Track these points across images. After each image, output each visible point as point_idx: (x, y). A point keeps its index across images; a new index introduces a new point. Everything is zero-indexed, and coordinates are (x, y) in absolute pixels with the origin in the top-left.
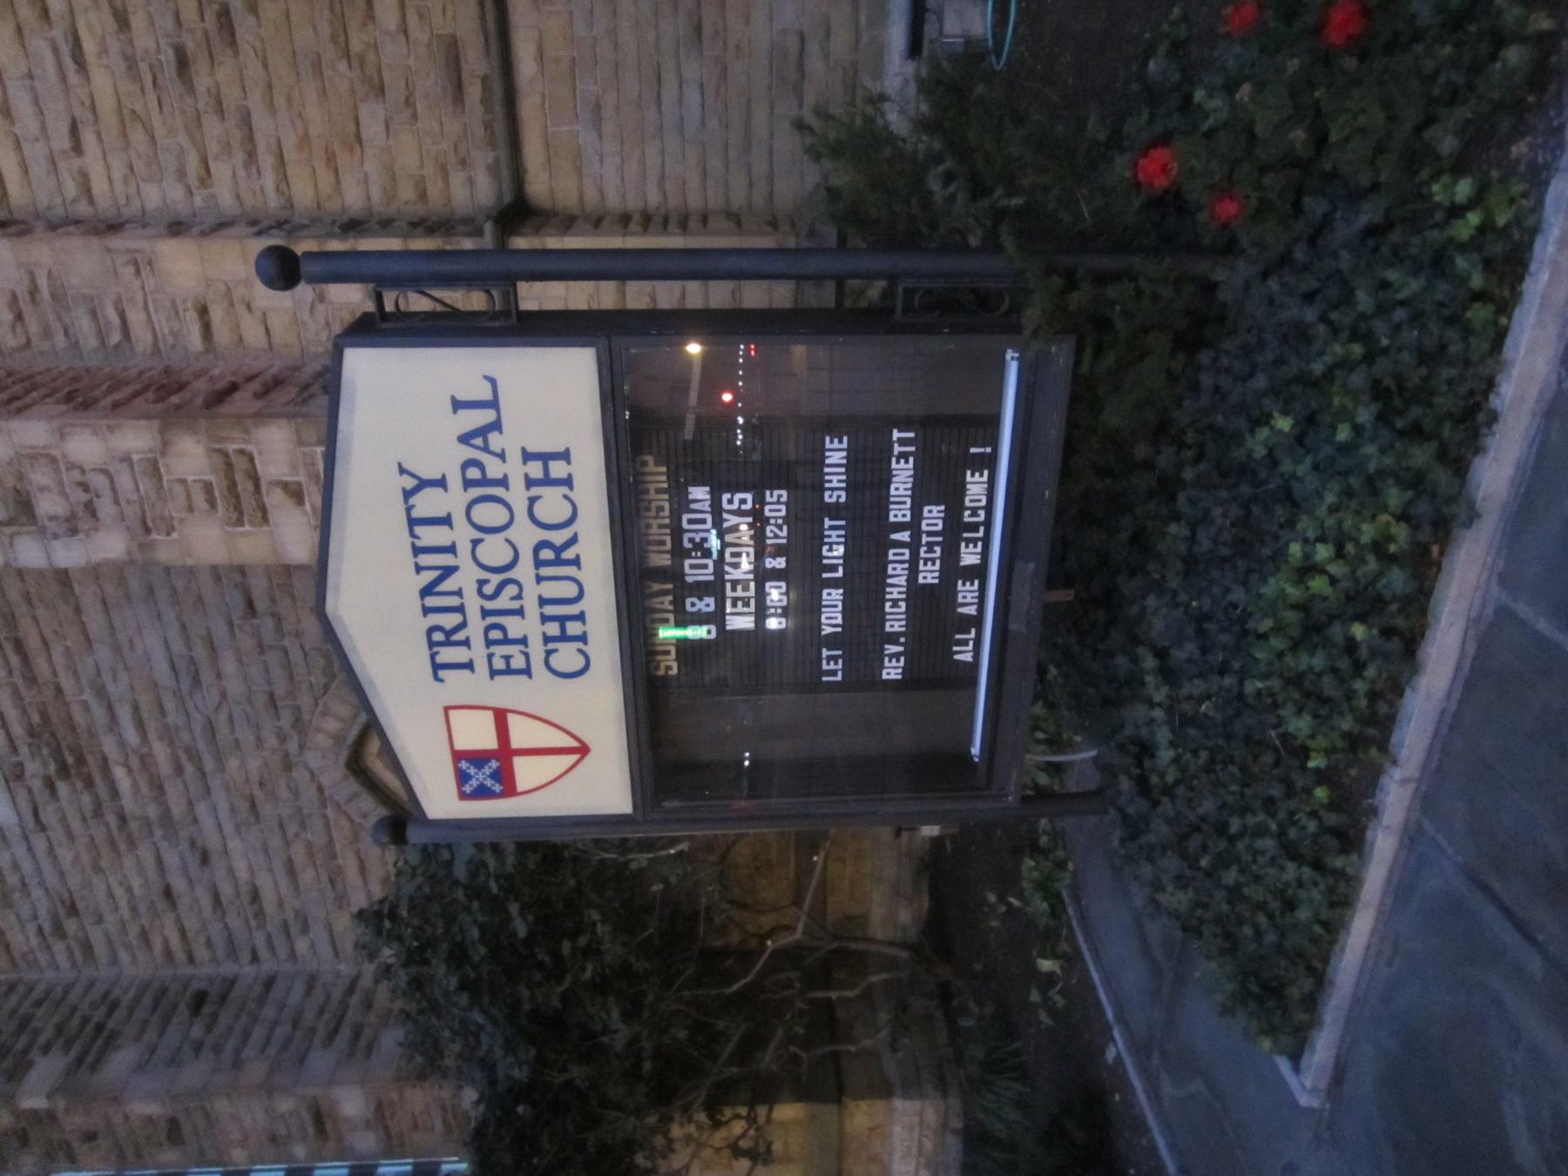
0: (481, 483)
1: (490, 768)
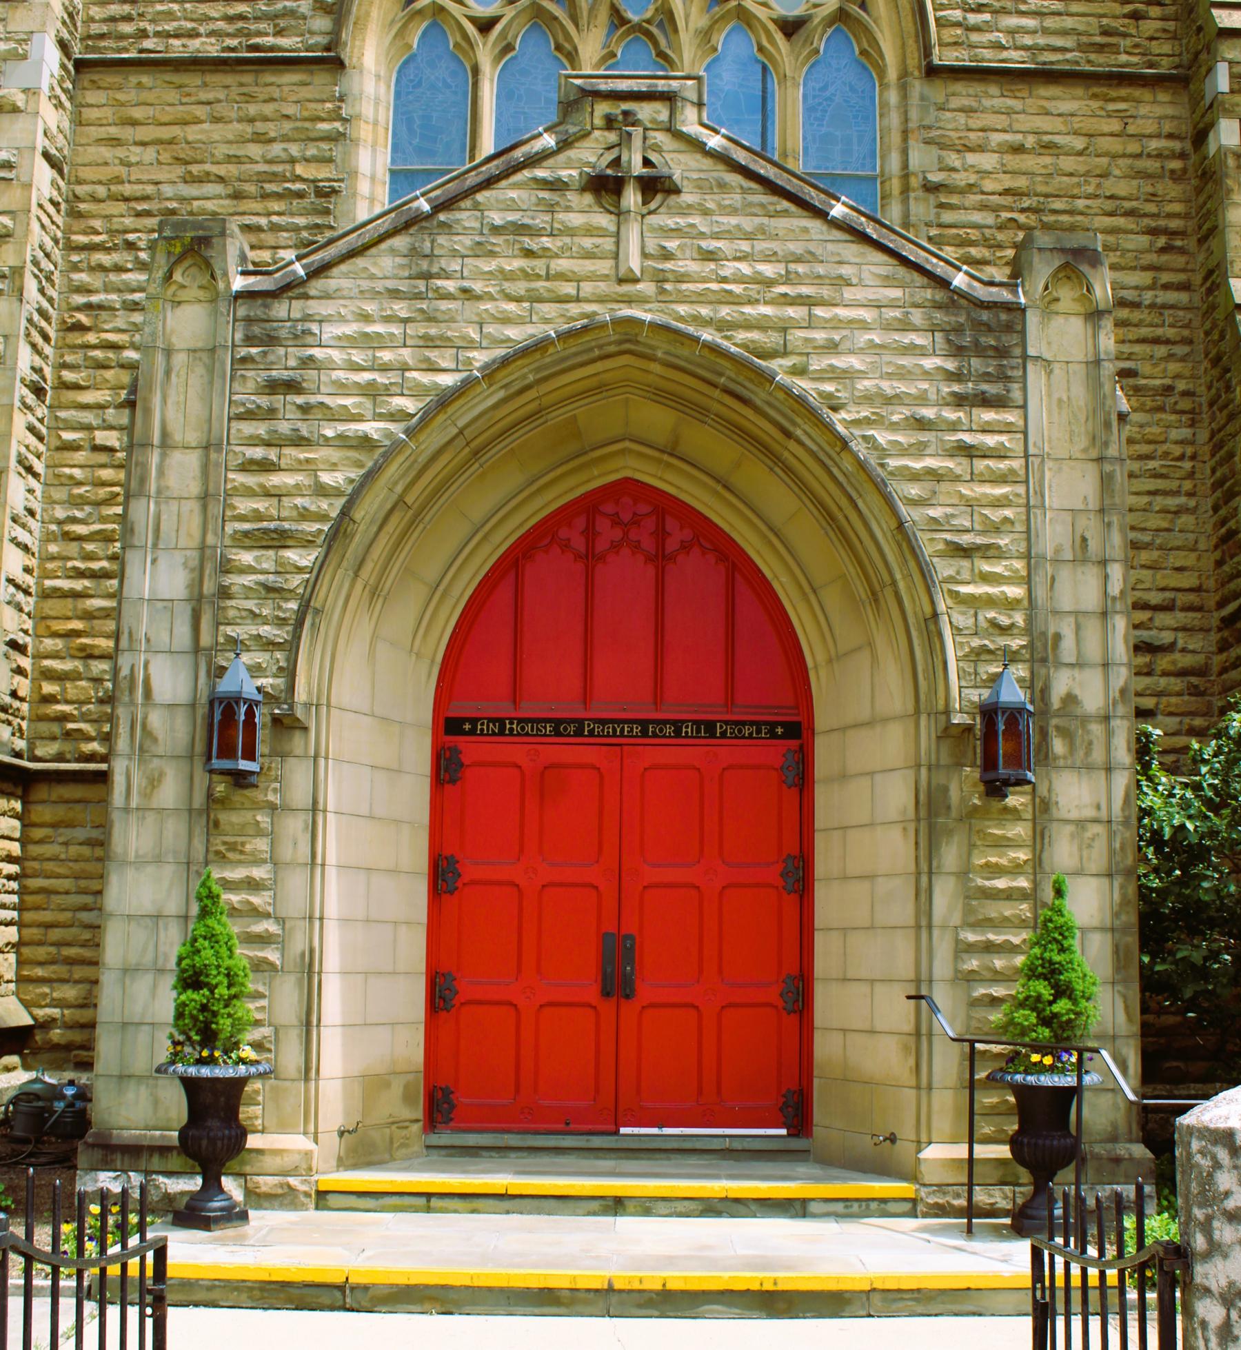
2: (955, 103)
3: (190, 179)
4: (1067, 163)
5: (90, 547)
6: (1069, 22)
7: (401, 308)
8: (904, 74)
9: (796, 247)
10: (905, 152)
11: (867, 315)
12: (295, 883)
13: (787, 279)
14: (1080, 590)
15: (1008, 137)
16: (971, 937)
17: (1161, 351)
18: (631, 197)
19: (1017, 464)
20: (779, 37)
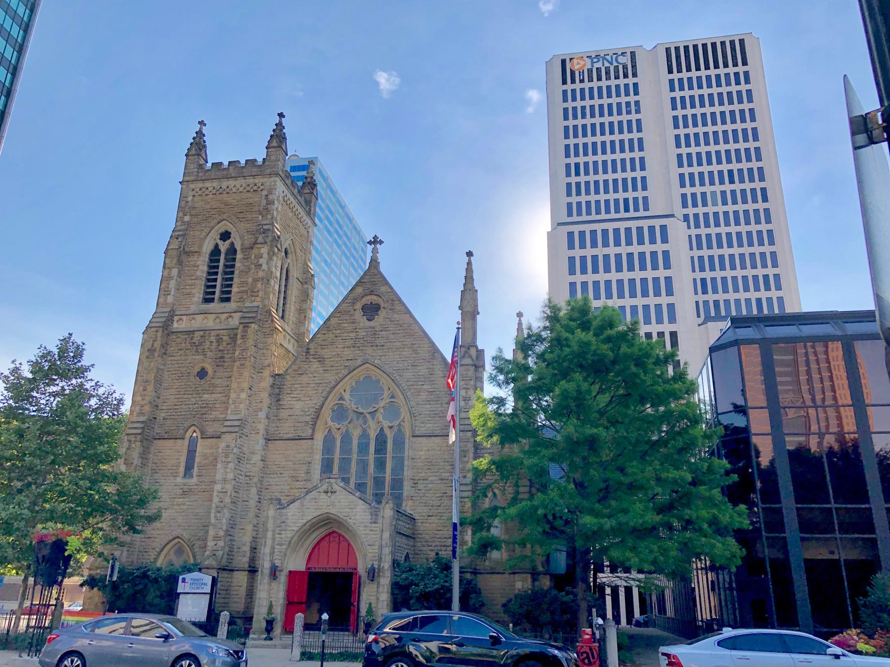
1: (184, 580)
3: (287, 461)
14: (387, 551)
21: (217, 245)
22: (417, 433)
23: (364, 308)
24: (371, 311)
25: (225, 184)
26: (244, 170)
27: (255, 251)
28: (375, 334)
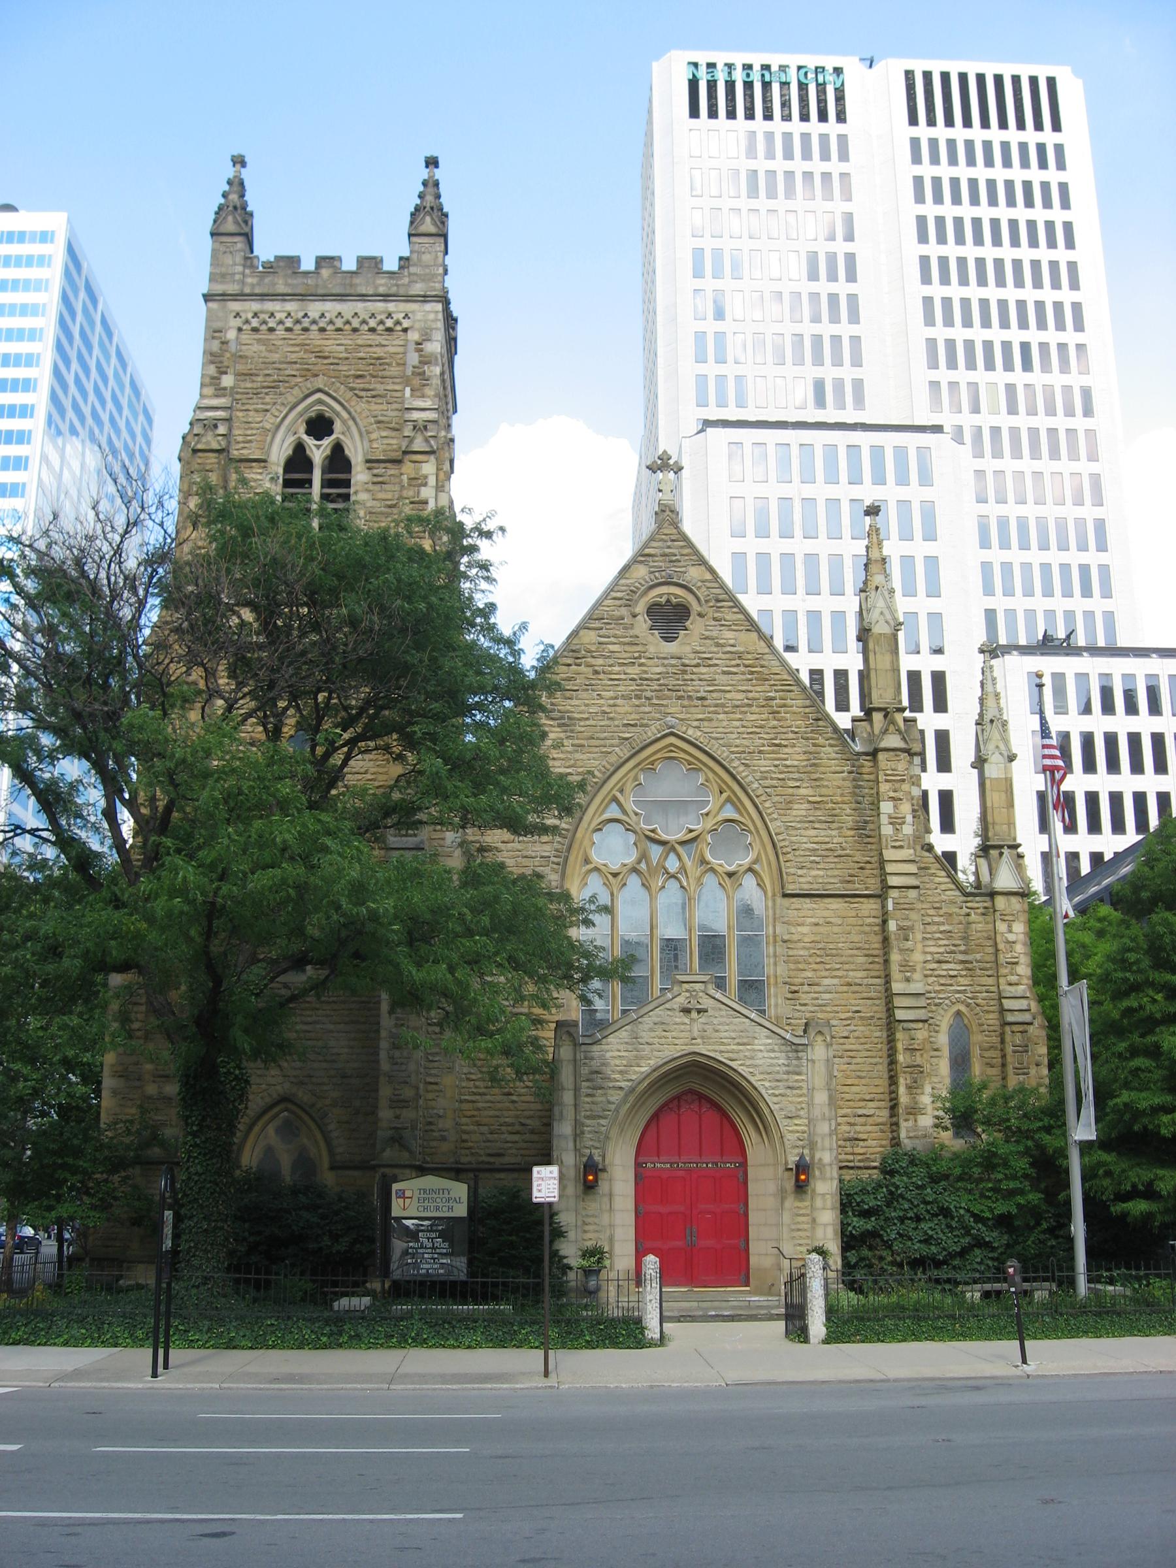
0: (449, 1200)
1: (402, 1195)
2: (793, 906)
4: (836, 929)
5: (477, 1083)
6: (836, 872)
7: (630, 1048)
8: (774, 895)
9: (741, 1028)
10: (774, 926)
11: (762, 1048)
12: (606, 1217)
13: (740, 1037)
14: (824, 1128)
15: (813, 920)
16: (793, 1227)
17: (869, 1002)
18: (694, 1014)
19: (805, 1091)
20: (726, 878)
21: (300, 448)
22: (791, 889)
23: (654, 610)
24: (670, 618)
25: (315, 309)
26: (357, 280)
27: (408, 468)
28: (685, 672)
